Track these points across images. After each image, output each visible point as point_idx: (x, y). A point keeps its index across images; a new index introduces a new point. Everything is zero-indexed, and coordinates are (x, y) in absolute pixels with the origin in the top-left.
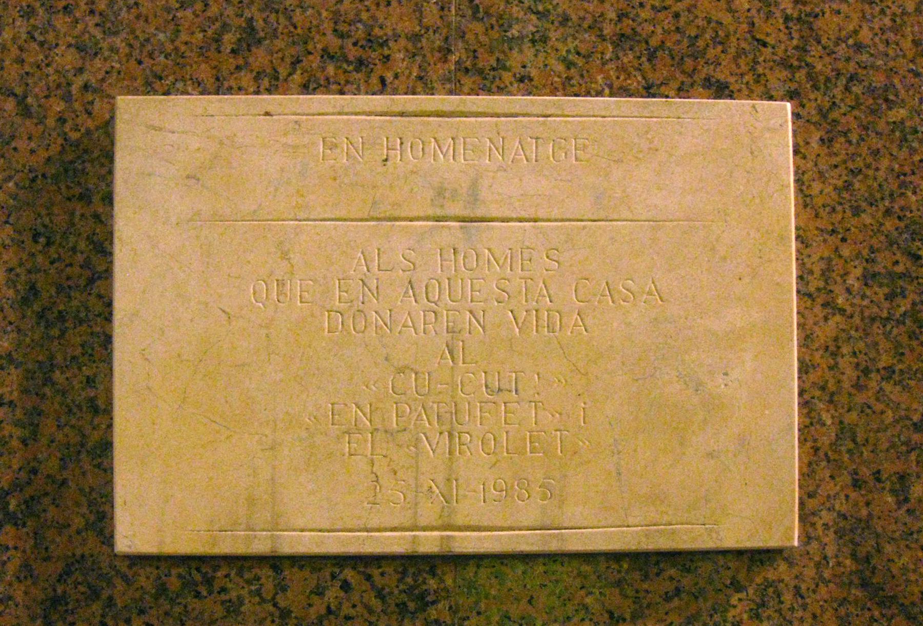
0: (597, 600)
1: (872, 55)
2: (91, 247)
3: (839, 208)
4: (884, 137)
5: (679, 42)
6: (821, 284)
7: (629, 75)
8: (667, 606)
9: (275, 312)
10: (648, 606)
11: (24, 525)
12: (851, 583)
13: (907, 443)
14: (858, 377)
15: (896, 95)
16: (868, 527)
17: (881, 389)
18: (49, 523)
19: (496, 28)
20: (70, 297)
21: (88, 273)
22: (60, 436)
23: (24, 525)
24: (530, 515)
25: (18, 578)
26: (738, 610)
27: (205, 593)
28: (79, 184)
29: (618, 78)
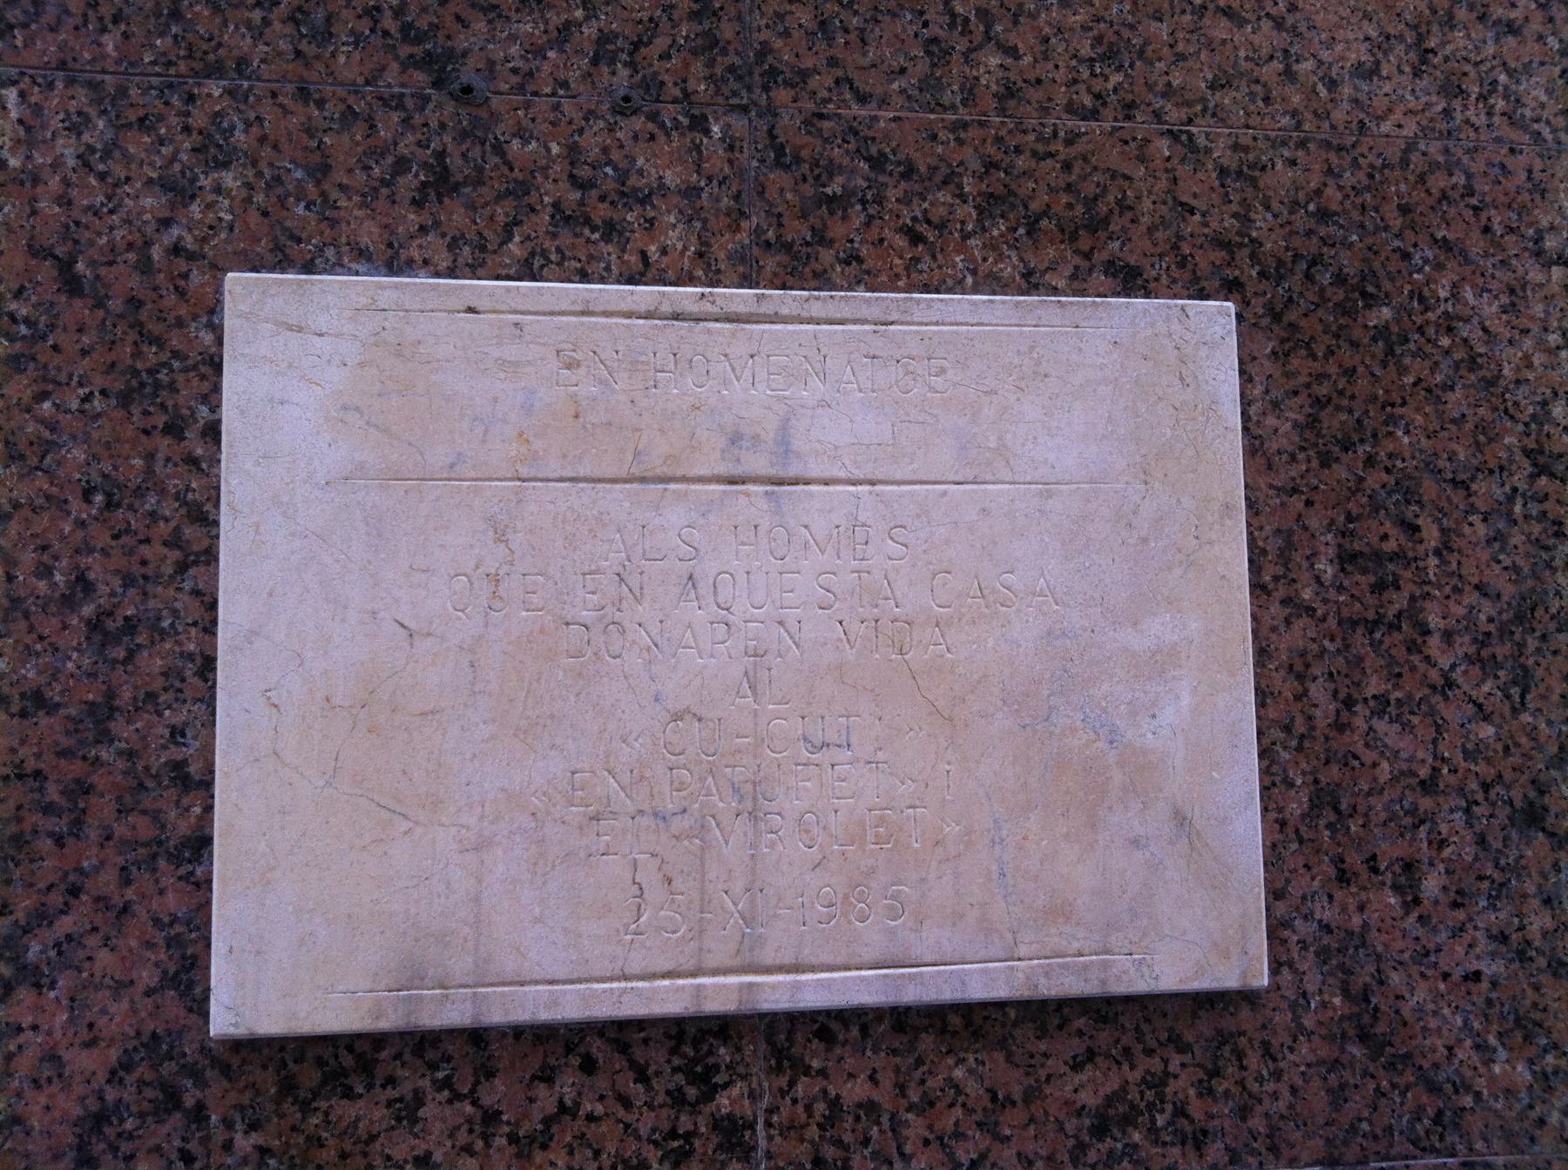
0: (971, 1071)
1: (1341, 227)
2: (183, 511)
3: (1301, 456)
4: (1361, 349)
5: (1070, 206)
6: (1280, 571)
7: (1001, 257)
8: (1080, 1078)
9: (486, 625)
10: (1049, 1078)
11: (52, 986)
12: (1344, 1035)
13: (1412, 812)
14: (1338, 711)
15: (1378, 287)
16: (1364, 944)
17: (1370, 728)
18: (97, 979)
19: (811, 180)
20: (145, 594)
21: (176, 554)
22: (120, 830)
23: (52, 986)
24: (873, 942)
25: (35, 1081)
26: (1181, 1082)
27: (360, 1089)
28: (163, 406)
29: (985, 260)
